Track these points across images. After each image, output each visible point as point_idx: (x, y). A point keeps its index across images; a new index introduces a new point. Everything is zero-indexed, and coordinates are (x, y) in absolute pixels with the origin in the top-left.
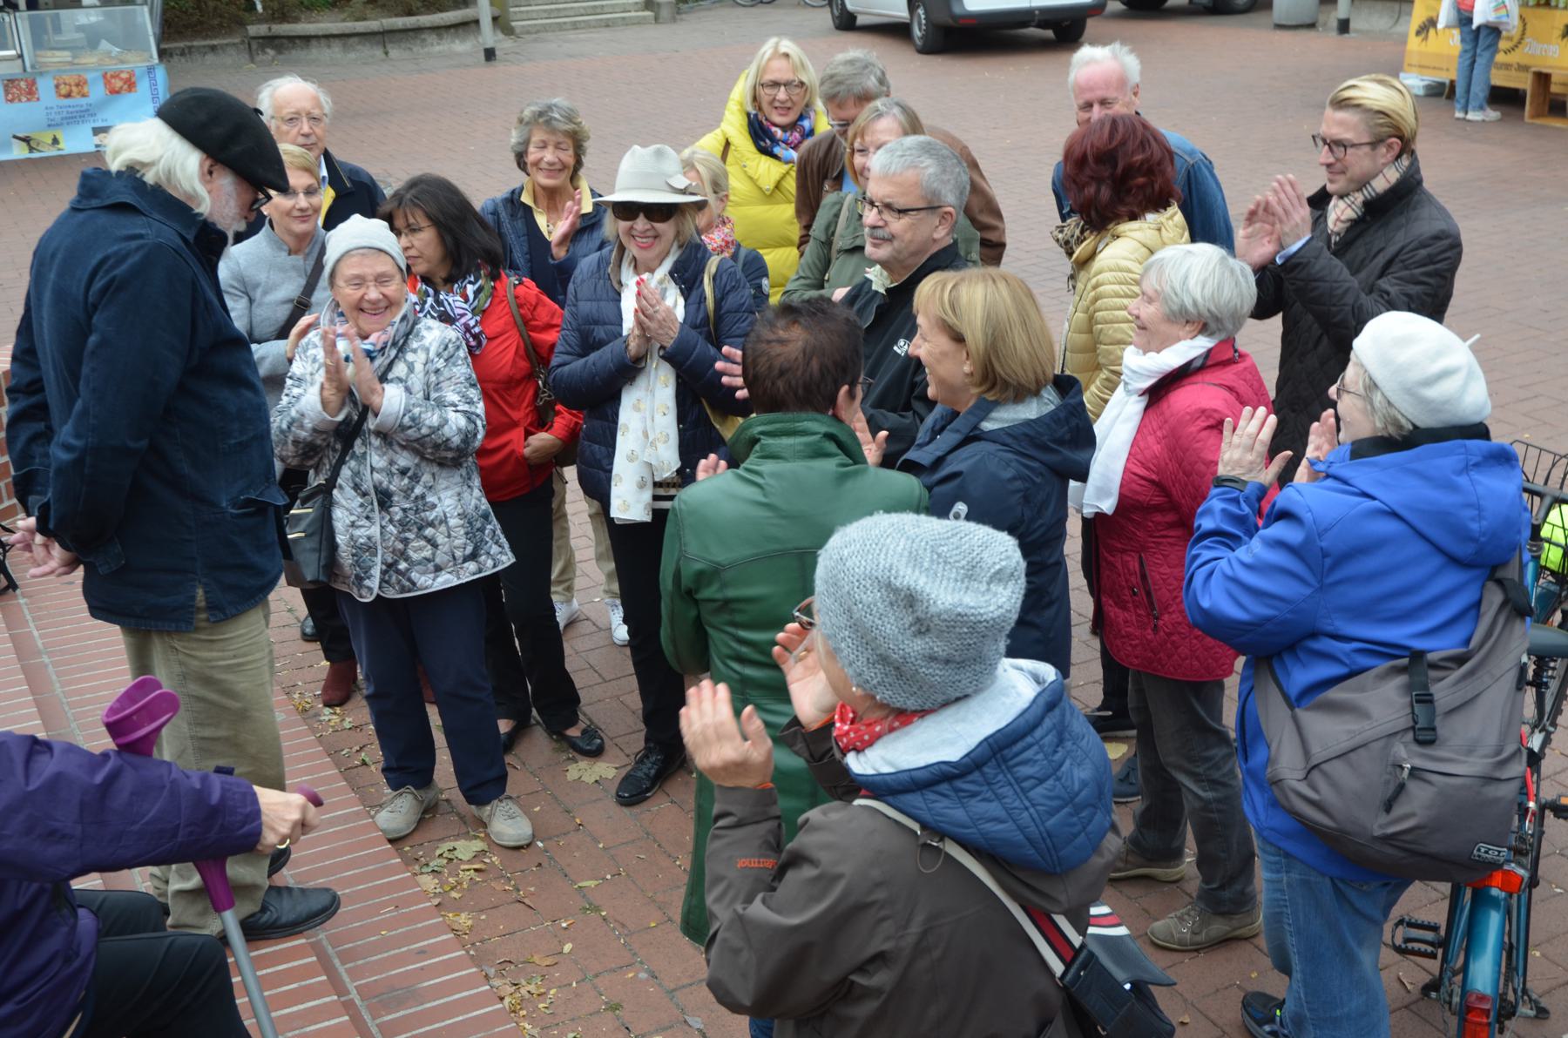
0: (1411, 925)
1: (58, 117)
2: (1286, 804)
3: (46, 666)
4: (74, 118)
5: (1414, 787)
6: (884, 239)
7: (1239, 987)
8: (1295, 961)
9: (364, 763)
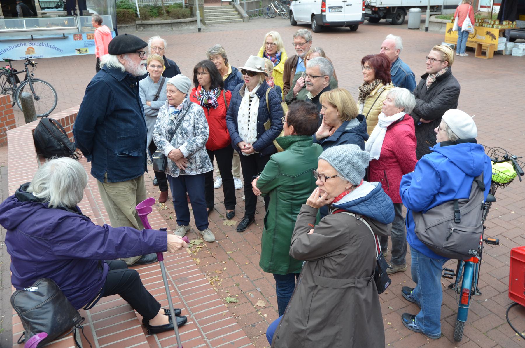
0: (447, 270)
1: (87, 44)
2: (420, 238)
3: (89, 190)
4: (92, 45)
5: (454, 234)
6: (310, 85)
7: (401, 285)
8: (419, 280)
9: (170, 218)
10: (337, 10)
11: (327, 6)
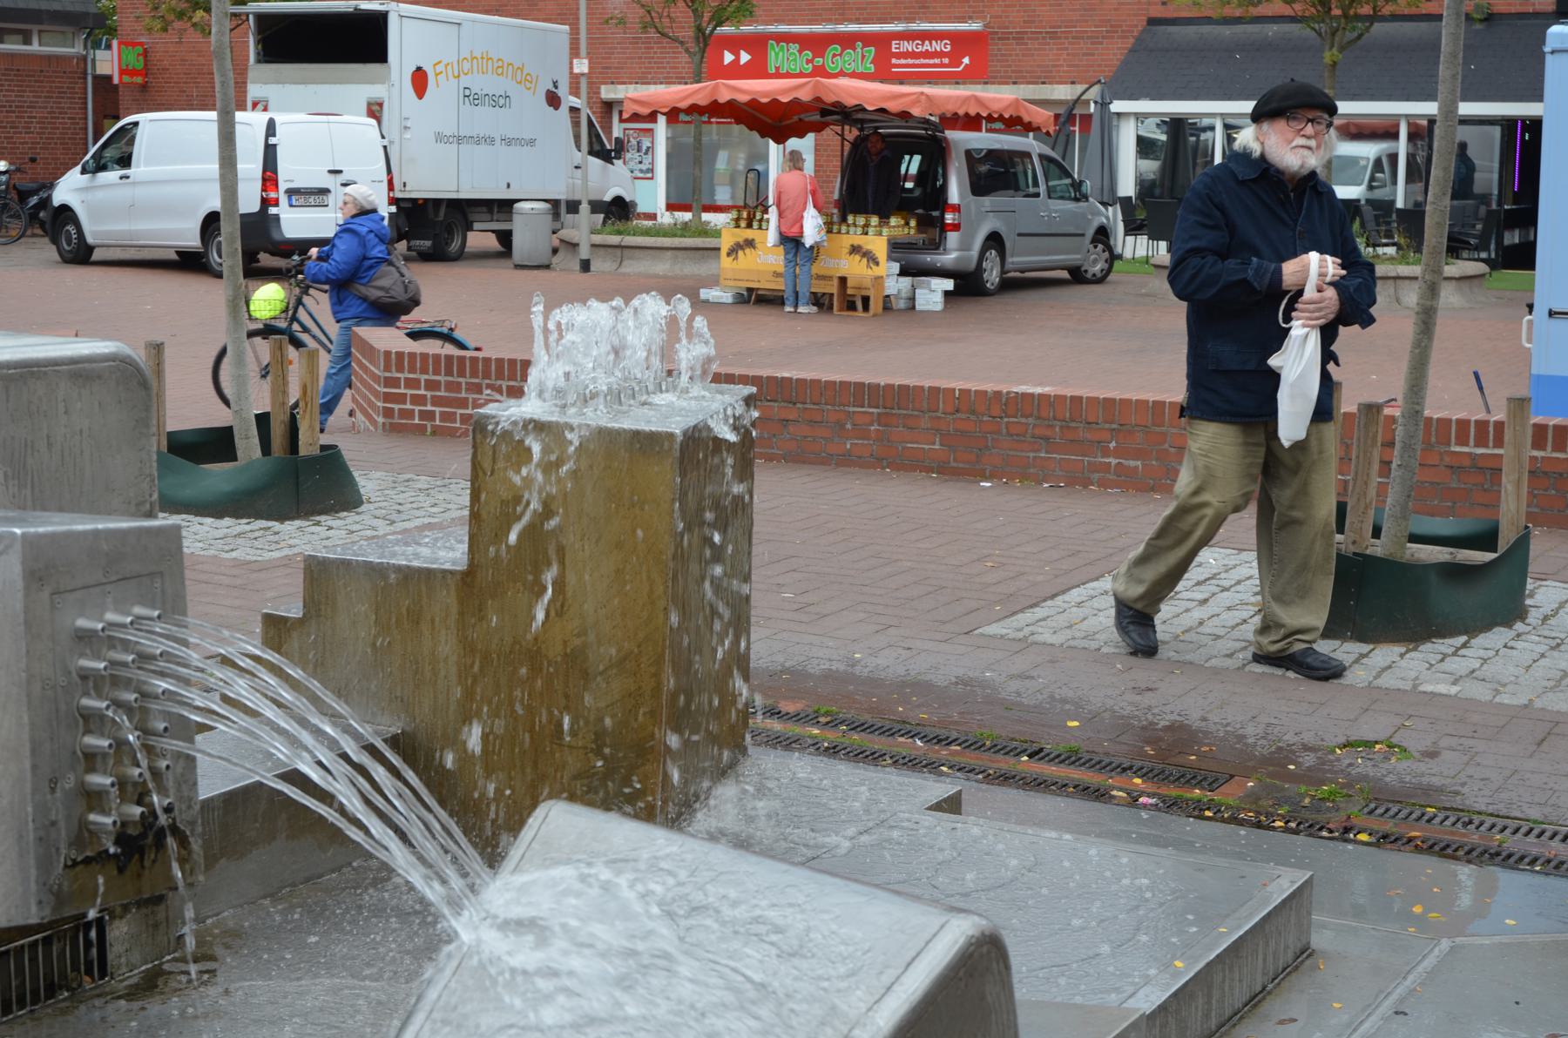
10: (312, 200)
11: (283, 186)
